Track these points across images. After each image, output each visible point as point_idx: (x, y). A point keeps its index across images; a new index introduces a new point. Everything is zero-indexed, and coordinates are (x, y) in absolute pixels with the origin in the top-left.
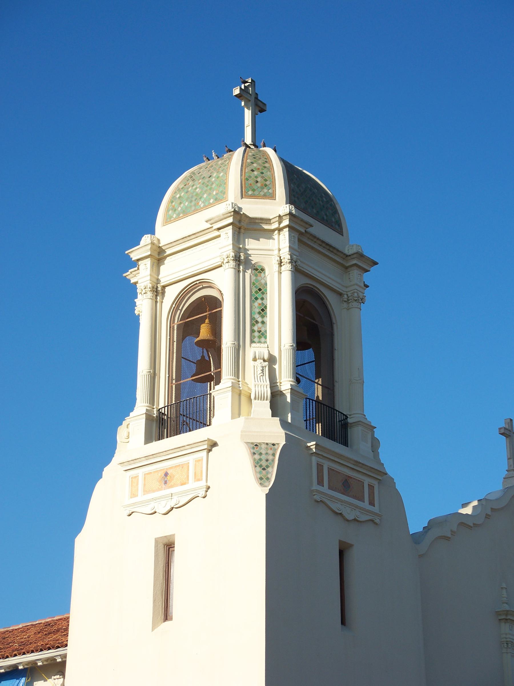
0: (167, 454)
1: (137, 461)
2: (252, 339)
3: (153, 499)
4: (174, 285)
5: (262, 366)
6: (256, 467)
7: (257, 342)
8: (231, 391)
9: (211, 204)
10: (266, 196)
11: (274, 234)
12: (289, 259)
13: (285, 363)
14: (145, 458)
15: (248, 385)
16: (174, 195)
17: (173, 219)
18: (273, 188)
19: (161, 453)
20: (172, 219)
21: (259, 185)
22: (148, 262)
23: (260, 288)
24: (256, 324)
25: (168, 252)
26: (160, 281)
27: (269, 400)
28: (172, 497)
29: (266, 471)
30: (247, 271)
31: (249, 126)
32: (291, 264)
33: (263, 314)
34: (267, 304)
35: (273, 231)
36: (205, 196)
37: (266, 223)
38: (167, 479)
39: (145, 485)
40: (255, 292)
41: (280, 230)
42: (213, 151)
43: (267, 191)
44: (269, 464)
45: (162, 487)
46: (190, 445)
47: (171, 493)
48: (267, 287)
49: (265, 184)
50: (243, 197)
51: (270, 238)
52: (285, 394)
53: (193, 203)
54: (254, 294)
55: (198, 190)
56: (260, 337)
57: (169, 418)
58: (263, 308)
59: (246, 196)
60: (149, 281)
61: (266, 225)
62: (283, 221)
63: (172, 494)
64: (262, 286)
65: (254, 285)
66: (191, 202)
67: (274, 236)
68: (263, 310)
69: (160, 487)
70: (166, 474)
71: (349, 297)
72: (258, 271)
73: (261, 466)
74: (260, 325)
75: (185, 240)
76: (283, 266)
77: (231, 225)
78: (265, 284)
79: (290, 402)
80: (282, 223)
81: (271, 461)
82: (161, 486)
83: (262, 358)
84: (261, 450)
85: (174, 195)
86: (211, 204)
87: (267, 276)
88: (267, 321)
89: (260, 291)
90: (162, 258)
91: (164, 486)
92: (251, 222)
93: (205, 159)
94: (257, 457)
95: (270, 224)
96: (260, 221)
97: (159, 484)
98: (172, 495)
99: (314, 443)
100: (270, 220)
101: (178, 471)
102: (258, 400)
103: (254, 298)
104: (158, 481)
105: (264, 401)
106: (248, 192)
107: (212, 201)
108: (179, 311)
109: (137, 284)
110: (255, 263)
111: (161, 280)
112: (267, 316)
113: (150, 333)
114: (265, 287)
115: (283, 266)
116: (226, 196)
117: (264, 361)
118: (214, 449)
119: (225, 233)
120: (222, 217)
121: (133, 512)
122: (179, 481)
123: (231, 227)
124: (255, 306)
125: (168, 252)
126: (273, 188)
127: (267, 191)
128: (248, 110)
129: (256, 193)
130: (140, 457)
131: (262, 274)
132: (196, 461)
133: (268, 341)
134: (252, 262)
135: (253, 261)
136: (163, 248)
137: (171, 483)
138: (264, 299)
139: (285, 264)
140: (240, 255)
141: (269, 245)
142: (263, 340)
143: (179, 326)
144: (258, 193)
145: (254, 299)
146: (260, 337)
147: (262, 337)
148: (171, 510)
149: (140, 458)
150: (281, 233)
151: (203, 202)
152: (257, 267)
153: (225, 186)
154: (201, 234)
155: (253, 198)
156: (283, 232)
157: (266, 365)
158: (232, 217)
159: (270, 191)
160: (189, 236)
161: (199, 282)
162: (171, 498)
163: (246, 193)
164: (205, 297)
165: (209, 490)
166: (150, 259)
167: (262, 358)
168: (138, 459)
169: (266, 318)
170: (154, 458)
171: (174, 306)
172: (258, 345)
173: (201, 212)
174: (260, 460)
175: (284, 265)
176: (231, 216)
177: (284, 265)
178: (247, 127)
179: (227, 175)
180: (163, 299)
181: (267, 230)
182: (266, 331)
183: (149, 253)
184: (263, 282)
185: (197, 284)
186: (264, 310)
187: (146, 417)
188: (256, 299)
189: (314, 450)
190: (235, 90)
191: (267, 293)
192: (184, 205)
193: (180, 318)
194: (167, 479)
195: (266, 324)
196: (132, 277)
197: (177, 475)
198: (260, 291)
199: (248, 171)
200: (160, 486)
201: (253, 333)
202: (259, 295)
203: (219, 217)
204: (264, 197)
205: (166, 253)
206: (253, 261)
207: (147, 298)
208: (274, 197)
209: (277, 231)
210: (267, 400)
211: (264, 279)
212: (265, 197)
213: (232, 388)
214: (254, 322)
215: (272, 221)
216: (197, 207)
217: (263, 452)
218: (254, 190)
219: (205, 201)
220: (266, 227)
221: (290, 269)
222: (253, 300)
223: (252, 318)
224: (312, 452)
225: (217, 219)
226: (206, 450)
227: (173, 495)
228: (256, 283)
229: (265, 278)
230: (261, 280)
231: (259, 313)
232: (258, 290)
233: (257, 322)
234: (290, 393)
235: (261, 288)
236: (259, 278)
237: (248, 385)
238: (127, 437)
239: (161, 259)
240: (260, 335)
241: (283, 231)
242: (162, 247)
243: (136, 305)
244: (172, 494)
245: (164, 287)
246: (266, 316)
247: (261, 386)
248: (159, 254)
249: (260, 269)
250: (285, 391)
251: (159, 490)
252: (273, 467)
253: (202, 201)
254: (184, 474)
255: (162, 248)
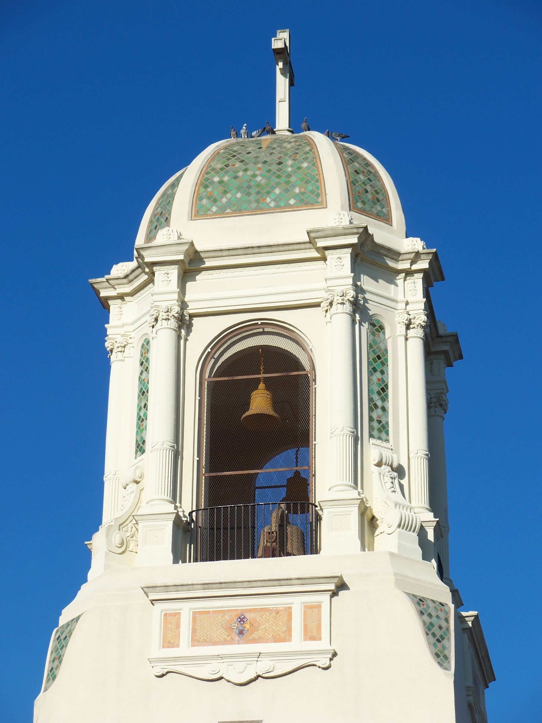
0: (249, 586)
1: (184, 588)
2: (371, 431)
3: (220, 656)
4: (210, 317)
5: (391, 476)
6: (427, 634)
7: (376, 438)
8: (358, 506)
9: (291, 206)
10: (379, 216)
11: (397, 276)
12: (425, 321)
13: (418, 480)
14: (202, 586)
15: (367, 502)
16: (206, 176)
17: (211, 213)
18: (388, 207)
19: (238, 583)
20: (209, 213)
21: (369, 196)
22: (174, 272)
23: (379, 355)
24: (374, 409)
25: (209, 263)
26: (188, 306)
27: (416, 533)
28: (258, 658)
29: (442, 644)
30: (363, 323)
31: (285, 101)
32: (423, 329)
33: (383, 396)
34: (388, 382)
35: (399, 272)
36: (277, 191)
37: (392, 259)
38: (245, 627)
39: (194, 631)
40: (372, 359)
41: (409, 273)
42: (245, 125)
43: (380, 209)
44: (444, 634)
45: (232, 639)
46: (302, 579)
47: (259, 652)
48: (387, 356)
49: (377, 197)
50: (351, 209)
51: (392, 281)
52: (424, 527)
53: (253, 197)
54: (371, 361)
55: (259, 179)
56: (380, 431)
57: (200, 527)
58: (383, 386)
59: (355, 209)
60: (176, 301)
61: (391, 260)
62: (418, 261)
63: (260, 653)
64: (381, 352)
65: (371, 349)
66: (249, 194)
67: (396, 280)
68: (384, 389)
69: (228, 639)
70: (242, 620)
71: (432, 398)
72: (376, 327)
73: (434, 635)
74: (379, 411)
75: (250, 251)
76: (411, 329)
77: (350, 248)
78: (384, 350)
79: (433, 541)
80: (415, 264)
81: (446, 630)
82: (232, 637)
83: (390, 464)
84: (430, 609)
85: (206, 176)
86: (291, 206)
87: (388, 339)
88: (388, 408)
89: (379, 360)
90: (192, 271)
91: (237, 638)
92: (373, 251)
93: (233, 133)
94: (425, 617)
95: (397, 260)
96: (385, 253)
97: (227, 634)
98: (259, 656)
99: (475, 613)
100: (399, 254)
101: (266, 617)
102: (403, 528)
103: (372, 368)
104: (223, 628)
105: (409, 532)
106: (357, 202)
107: (292, 202)
108: (213, 360)
109: (109, 300)
110: (373, 315)
111: (188, 304)
112: (388, 401)
113: (174, 385)
114: (385, 356)
115: (411, 329)
116: (322, 200)
117: (393, 469)
118: (341, 593)
119: (338, 258)
120: (341, 231)
121: (168, 673)
122: (271, 635)
123: (349, 250)
124: (373, 382)
125: (209, 263)
126: (388, 207)
127: (380, 209)
128: (285, 77)
129: (367, 207)
130: (194, 582)
131: (381, 334)
132: (305, 607)
133: (390, 438)
134: (369, 311)
135: (370, 310)
136: (202, 255)
137: (254, 635)
138: (385, 373)
139: (416, 327)
140: (358, 296)
141: (390, 292)
142: (383, 435)
143: (209, 383)
144: (370, 209)
145: (371, 369)
146: (380, 431)
147: (382, 431)
148: (254, 679)
149: (192, 585)
150: (408, 278)
151: (274, 200)
152: (374, 322)
153: (318, 184)
154: (281, 248)
155: (364, 214)
156: (413, 278)
157: (396, 477)
158: (357, 236)
159: (384, 210)
160: (259, 247)
161: (261, 323)
162: (256, 659)
163: (354, 204)
164: (266, 349)
165: (335, 658)
166: (177, 266)
167: (390, 464)
168: (189, 586)
169: (387, 403)
170: (222, 589)
171: (209, 350)
172: (378, 442)
173: (271, 214)
174: (431, 624)
175: (414, 328)
176: (357, 233)
177: (414, 328)
178: (279, 102)
179: (317, 168)
180: (188, 334)
181: (390, 269)
182: (387, 423)
183: (181, 257)
184: (382, 346)
185: (257, 324)
186: (385, 391)
187: (174, 519)
188: (375, 370)
189: (470, 624)
190: (274, 40)
191: (387, 365)
192: (234, 195)
193: (215, 370)
194: (245, 627)
195: (388, 412)
196: (104, 287)
197: (267, 624)
198: (379, 360)
199: (351, 171)
200: (228, 636)
201: (372, 422)
202: (377, 365)
203: (335, 231)
204: (377, 217)
205: (204, 265)
206: (370, 310)
207: (169, 327)
208: (390, 221)
209: (404, 274)
210: (414, 531)
211: (383, 342)
212: (379, 218)
213: (360, 502)
214: (373, 407)
215: (401, 258)
216: (262, 205)
217: (434, 614)
218: (364, 203)
219: (278, 199)
220: (391, 264)
221: (422, 337)
222: (371, 370)
223: (370, 400)
224: (466, 627)
225: (329, 232)
226: (331, 592)
227: (261, 655)
228: (374, 346)
229: (384, 342)
230: (380, 343)
231: (379, 393)
232: (376, 357)
233: (376, 406)
234: (433, 528)
235: (381, 356)
236: (377, 339)
237: (368, 501)
238: (120, 544)
239: (189, 271)
240: (380, 427)
241: (413, 276)
242: (201, 254)
243: (108, 334)
244: (260, 653)
245: (192, 316)
246: (387, 400)
247: (403, 507)
248: (191, 262)
249: (379, 325)
250: (426, 523)
251: (225, 642)
252: (449, 639)
253: (273, 198)
254: (281, 624)
255: (200, 255)
